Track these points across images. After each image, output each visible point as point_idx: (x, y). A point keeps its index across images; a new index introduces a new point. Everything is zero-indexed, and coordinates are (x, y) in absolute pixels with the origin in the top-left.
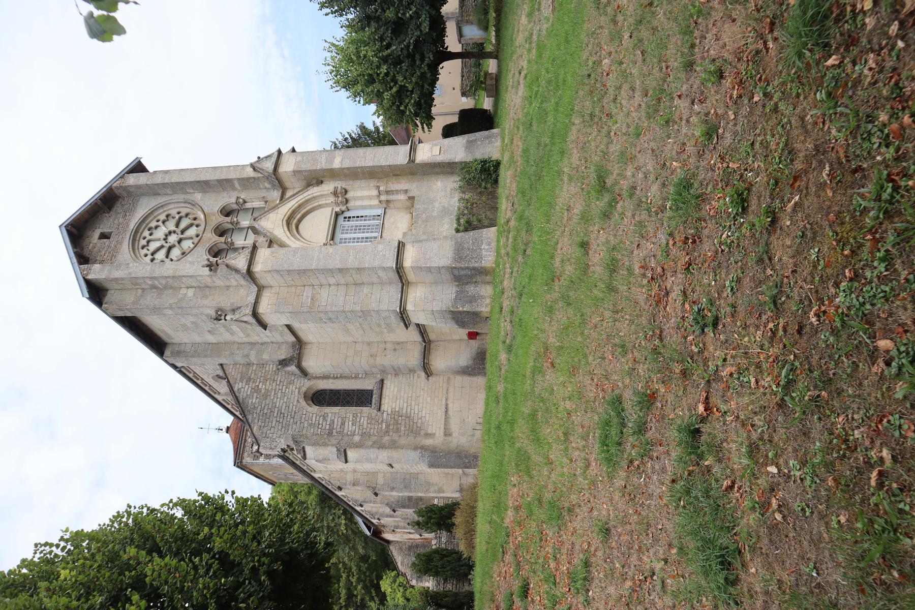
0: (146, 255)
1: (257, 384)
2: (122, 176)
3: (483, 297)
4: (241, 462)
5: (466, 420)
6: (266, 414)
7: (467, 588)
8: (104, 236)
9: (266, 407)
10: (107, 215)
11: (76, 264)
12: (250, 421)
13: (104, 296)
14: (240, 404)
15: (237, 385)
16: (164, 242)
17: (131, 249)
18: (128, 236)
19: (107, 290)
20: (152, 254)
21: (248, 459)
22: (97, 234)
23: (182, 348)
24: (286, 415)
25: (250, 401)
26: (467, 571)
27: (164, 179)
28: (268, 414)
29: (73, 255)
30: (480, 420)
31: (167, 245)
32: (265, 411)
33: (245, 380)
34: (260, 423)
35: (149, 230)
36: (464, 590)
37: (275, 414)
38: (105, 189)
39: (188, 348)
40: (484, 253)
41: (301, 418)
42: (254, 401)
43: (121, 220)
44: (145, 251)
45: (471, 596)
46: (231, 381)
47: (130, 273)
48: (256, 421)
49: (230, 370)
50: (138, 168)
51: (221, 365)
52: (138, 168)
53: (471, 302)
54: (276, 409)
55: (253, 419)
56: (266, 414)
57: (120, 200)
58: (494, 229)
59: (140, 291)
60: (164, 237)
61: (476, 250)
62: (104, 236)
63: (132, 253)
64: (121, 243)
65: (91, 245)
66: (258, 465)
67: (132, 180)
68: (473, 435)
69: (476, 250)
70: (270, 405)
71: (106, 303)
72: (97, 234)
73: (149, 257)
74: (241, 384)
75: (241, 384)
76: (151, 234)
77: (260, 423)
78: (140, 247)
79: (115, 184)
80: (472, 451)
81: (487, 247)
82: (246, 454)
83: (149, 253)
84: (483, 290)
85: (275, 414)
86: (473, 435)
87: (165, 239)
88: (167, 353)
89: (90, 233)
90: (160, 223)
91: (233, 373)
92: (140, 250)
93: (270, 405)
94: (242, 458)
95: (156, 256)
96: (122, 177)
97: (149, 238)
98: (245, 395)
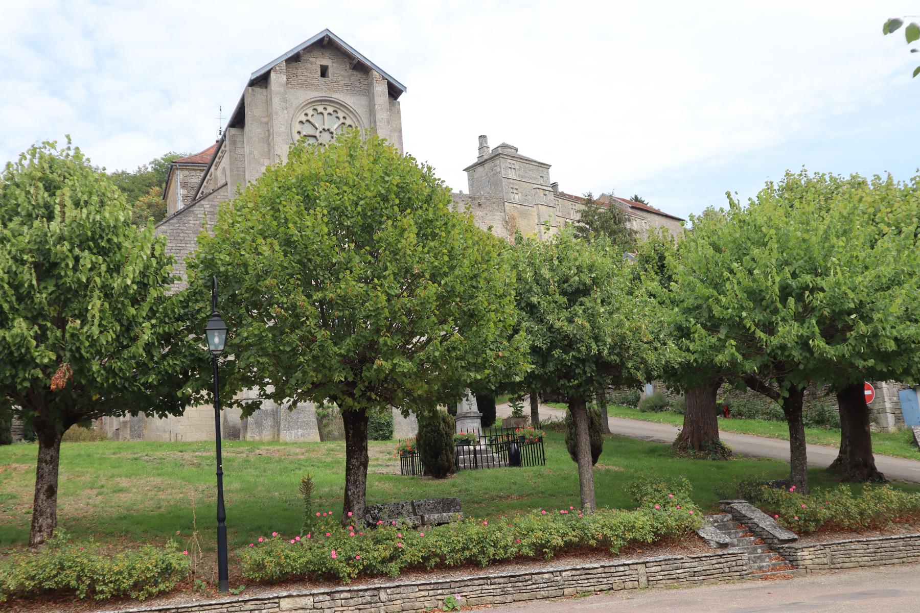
0: (306, 115)
1: (209, 222)
2: (385, 77)
3: (260, 433)
4: (177, 169)
5: (180, 424)
6: (179, 236)
7: (14, 438)
8: (324, 72)
9: (186, 235)
10: (348, 66)
11: (286, 58)
12: (171, 221)
13: (261, 87)
14: (187, 209)
15: (207, 203)
16: (321, 129)
17: (309, 101)
18: (324, 95)
19: (266, 88)
20: (308, 121)
21: (182, 176)
22: (326, 62)
23: (239, 145)
24: (178, 255)
25: (191, 219)
26: (29, 437)
27: (381, 121)
28: (179, 238)
29: (296, 51)
30: (179, 437)
31: (317, 134)
32: (181, 235)
33: (212, 210)
34: (169, 231)
35: (335, 111)
36: (12, 436)
37: (179, 245)
38: (369, 64)
39: (239, 151)
40: (293, 432)
41: (176, 270)
42: (191, 222)
43: (342, 83)
44: (310, 112)
45: (8, 442)
46: (210, 197)
47: (277, 113)
48: (171, 227)
49: (222, 194)
50: (394, 91)
51: (227, 184)
52: (394, 91)
53: (256, 423)
54: (183, 245)
55: (173, 224)
56: (179, 236)
57: (364, 77)
58: (318, 438)
59: (266, 120)
60: (326, 129)
61: (297, 424)
62: (324, 72)
63: (306, 102)
64: (316, 90)
65: (314, 60)
66: (176, 188)
67: (381, 89)
68: (165, 431)
69: (297, 424)
70: (188, 239)
71: (253, 90)
72: (326, 62)
73: (304, 119)
74: (208, 206)
75: (208, 206)
76: (329, 114)
77: (169, 231)
78: (315, 107)
79: (375, 73)
80: (146, 432)
81: (299, 434)
82: (186, 173)
83: (309, 118)
84: (267, 433)
85: (179, 245)
86: (165, 431)
87: (324, 129)
88: (234, 131)
89: (327, 54)
90: (342, 120)
91: (219, 197)
92: (312, 108)
93: (188, 239)
94: (182, 169)
95: (307, 124)
96: (384, 78)
97: (325, 113)
98: (197, 212)
